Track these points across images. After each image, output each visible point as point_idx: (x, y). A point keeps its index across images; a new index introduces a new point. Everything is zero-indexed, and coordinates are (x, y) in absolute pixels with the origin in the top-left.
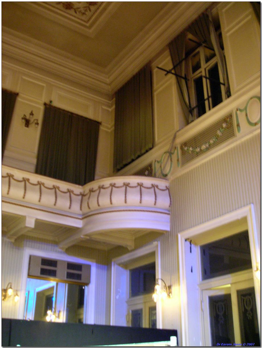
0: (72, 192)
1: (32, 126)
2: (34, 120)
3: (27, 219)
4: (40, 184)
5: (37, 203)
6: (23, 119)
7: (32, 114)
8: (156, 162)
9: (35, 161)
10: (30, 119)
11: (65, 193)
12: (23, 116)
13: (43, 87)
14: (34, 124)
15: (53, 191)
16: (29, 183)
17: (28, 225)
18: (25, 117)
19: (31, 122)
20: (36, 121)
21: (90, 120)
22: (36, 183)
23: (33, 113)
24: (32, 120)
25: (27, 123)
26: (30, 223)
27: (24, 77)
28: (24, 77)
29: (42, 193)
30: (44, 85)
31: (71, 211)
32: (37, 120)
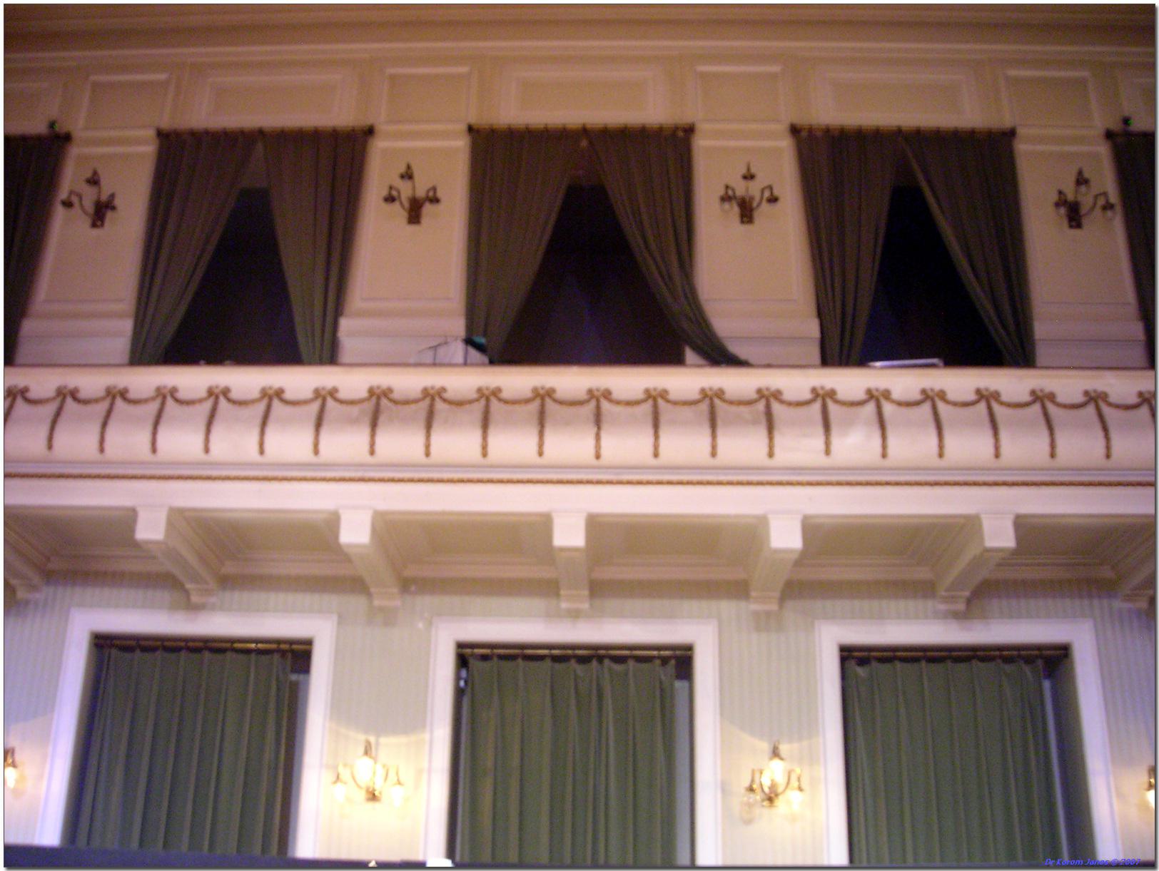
0: (1052, 397)
1: (764, 212)
2: (762, 191)
3: (987, 525)
4: (930, 398)
5: (936, 462)
6: (1057, 205)
7: (1081, 181)
8: (396, 197)
9: (813, 329)
10: (1080, 199)
11: (916, 404)
12: (1055, 198)
13: (1083, 82)
14: (764, 203)
15: (1036, 408)
16: (1002, 403)
17: (990, 542)
18: (1063, 197)
19: (1083, 210)
20: (767, 194)
21: (972, 133)
22: (1079, 398)
23: (1086, 175)
24: (1086, 201)
25: (1074, 216)
26: (1000, 536)
27: (1013, 73)
28: (1013, 73)
29: (719, 422)
30: (1085, 73)
31: (719, 460)
32: (770, 188)
